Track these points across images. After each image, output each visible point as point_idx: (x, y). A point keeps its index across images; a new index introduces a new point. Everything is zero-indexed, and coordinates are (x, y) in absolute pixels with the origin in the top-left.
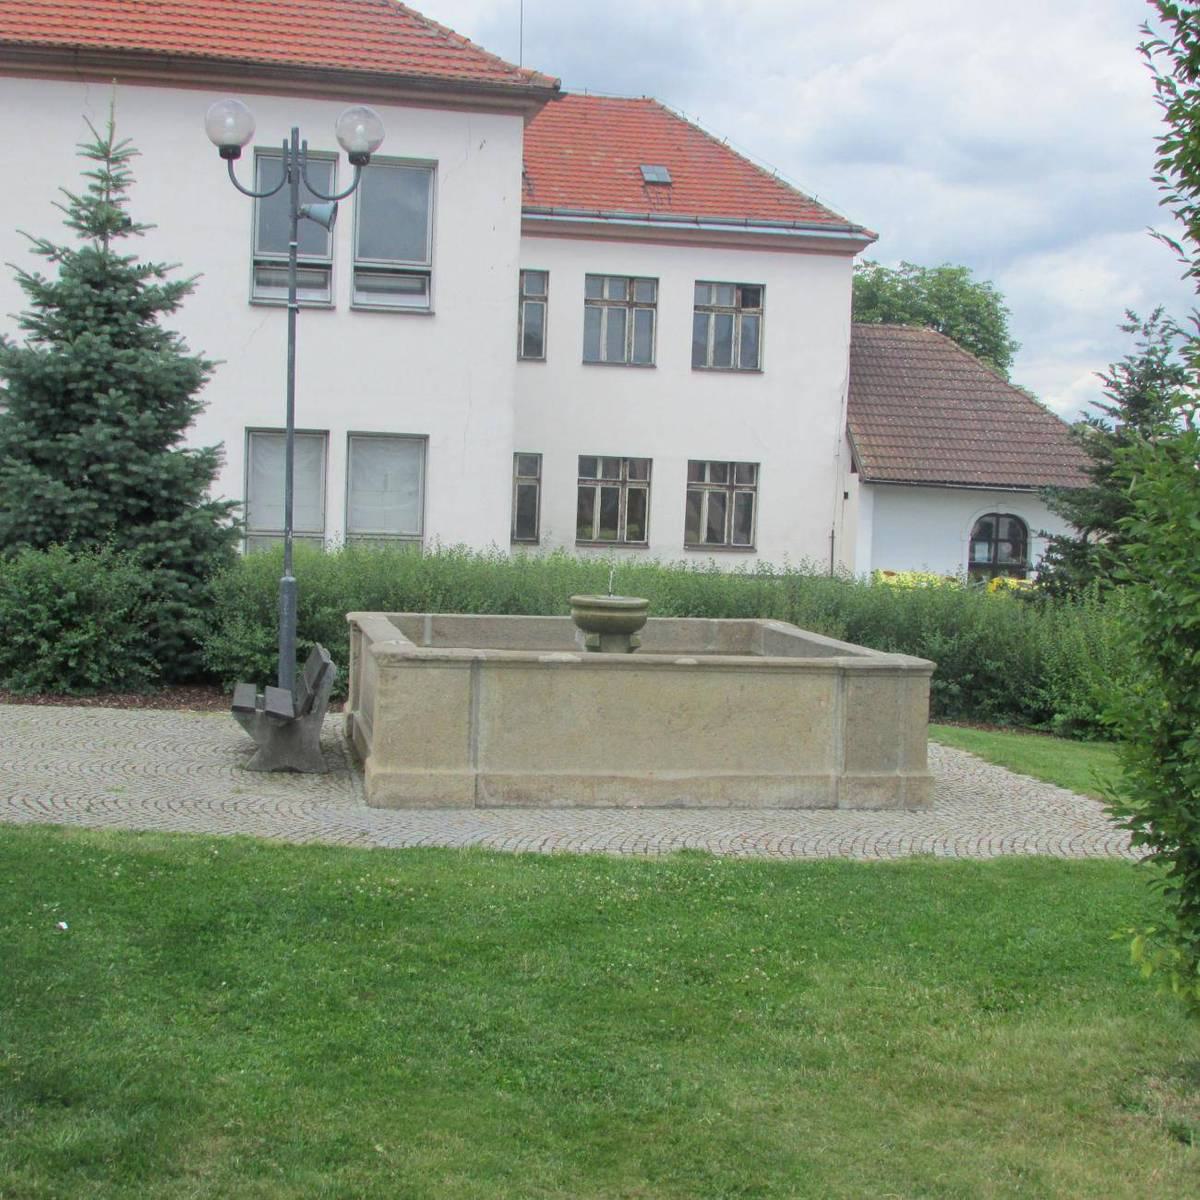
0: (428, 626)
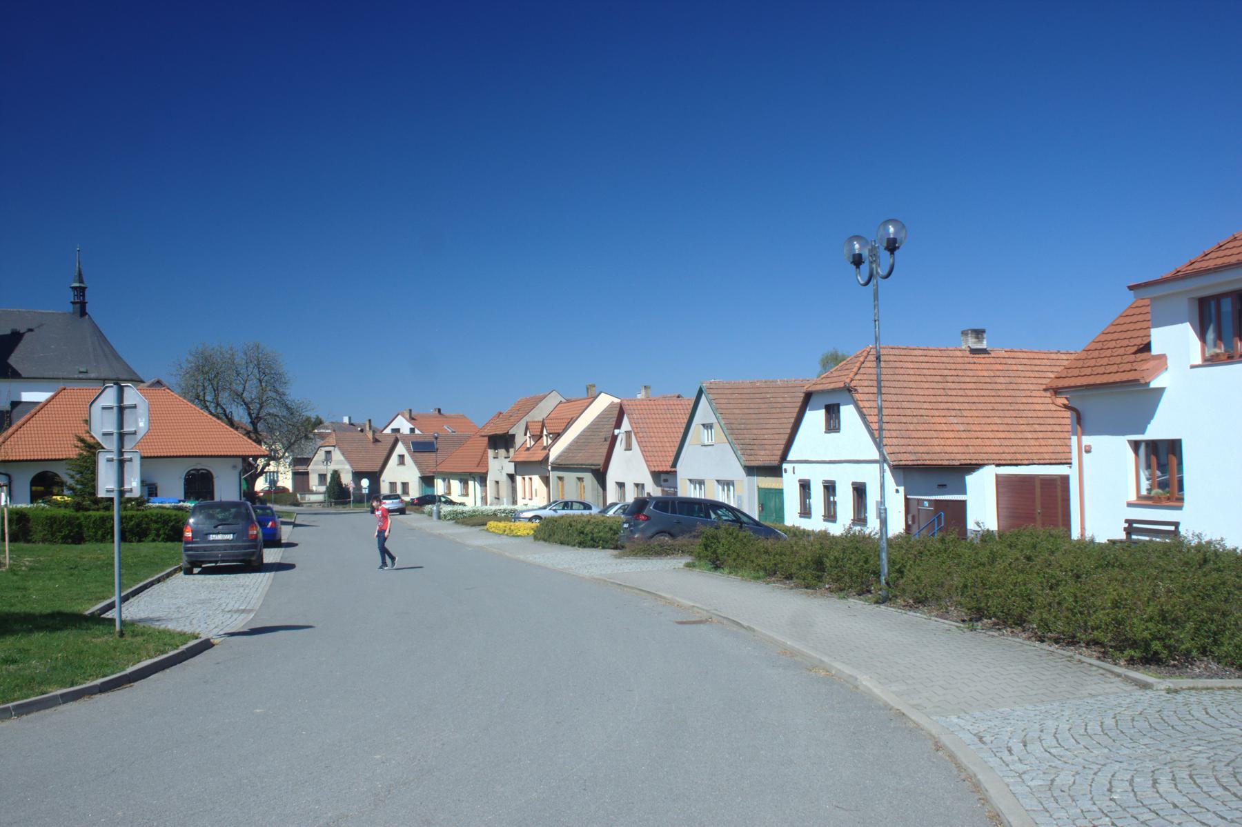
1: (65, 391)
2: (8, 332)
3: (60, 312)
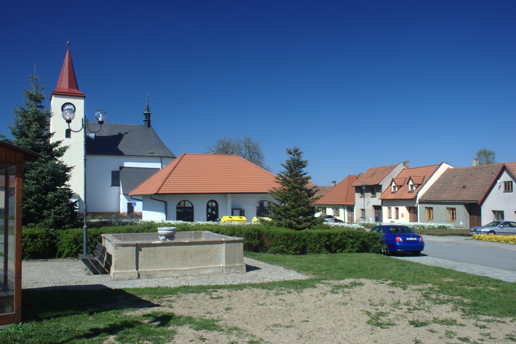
0: (122, 237)
1: (186, 155)
2: (117, 134)
3: (139, 125)
